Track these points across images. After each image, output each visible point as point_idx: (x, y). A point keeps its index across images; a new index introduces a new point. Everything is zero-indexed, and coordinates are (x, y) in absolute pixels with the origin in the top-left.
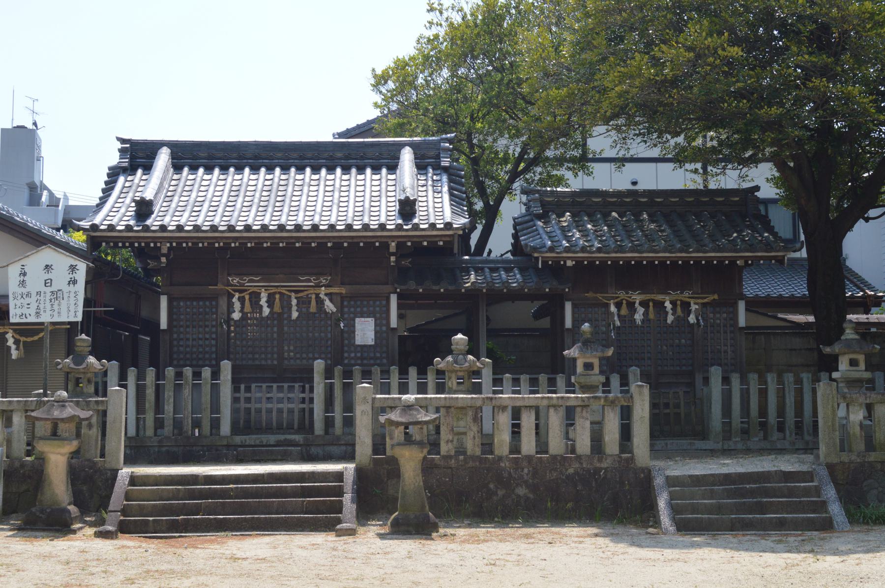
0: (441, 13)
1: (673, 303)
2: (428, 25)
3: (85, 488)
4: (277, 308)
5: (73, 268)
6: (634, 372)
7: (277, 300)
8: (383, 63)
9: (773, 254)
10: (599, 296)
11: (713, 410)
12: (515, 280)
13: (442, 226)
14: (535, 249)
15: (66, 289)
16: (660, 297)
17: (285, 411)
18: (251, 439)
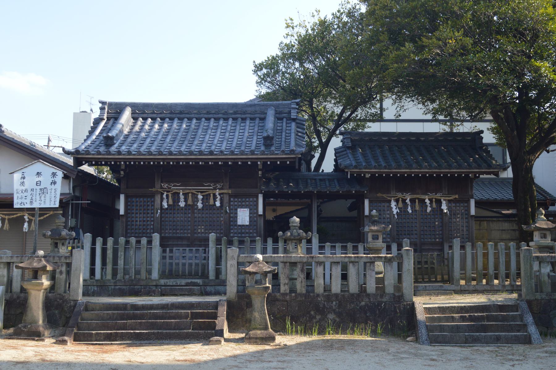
0: (293, 28)
1: (431, 200)
2: (285, 36)
3: (57, 312)
4: (190, 202)
5: (54, 174)
6: (406, 241)
7: (190, 197)
8: (262, 58)
9: (492, 170)
10: (384, 195)
11: (455, 266)
12: (336, 188)
13: (288, 152)
14: (346, 167)
15: (49, 187)
16: (423, 197)
17: (194, 264)
18: (170, 282)
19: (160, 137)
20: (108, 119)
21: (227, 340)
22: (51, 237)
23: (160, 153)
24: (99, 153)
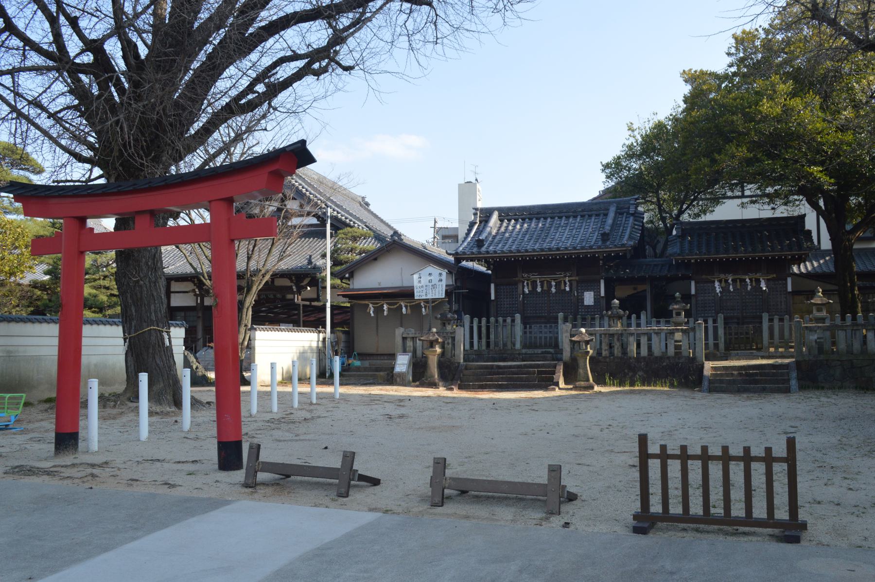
4: (545, 288)
5: (440, 274)
8: (608, 159)
15: (438, 283)
16: (744, 277)
18: (530, 351)
19: (520, 237)
20: (481, 222)
21: (560, 389)
22: (440, 319)
23: (519, 251)
24: (473, 253)
